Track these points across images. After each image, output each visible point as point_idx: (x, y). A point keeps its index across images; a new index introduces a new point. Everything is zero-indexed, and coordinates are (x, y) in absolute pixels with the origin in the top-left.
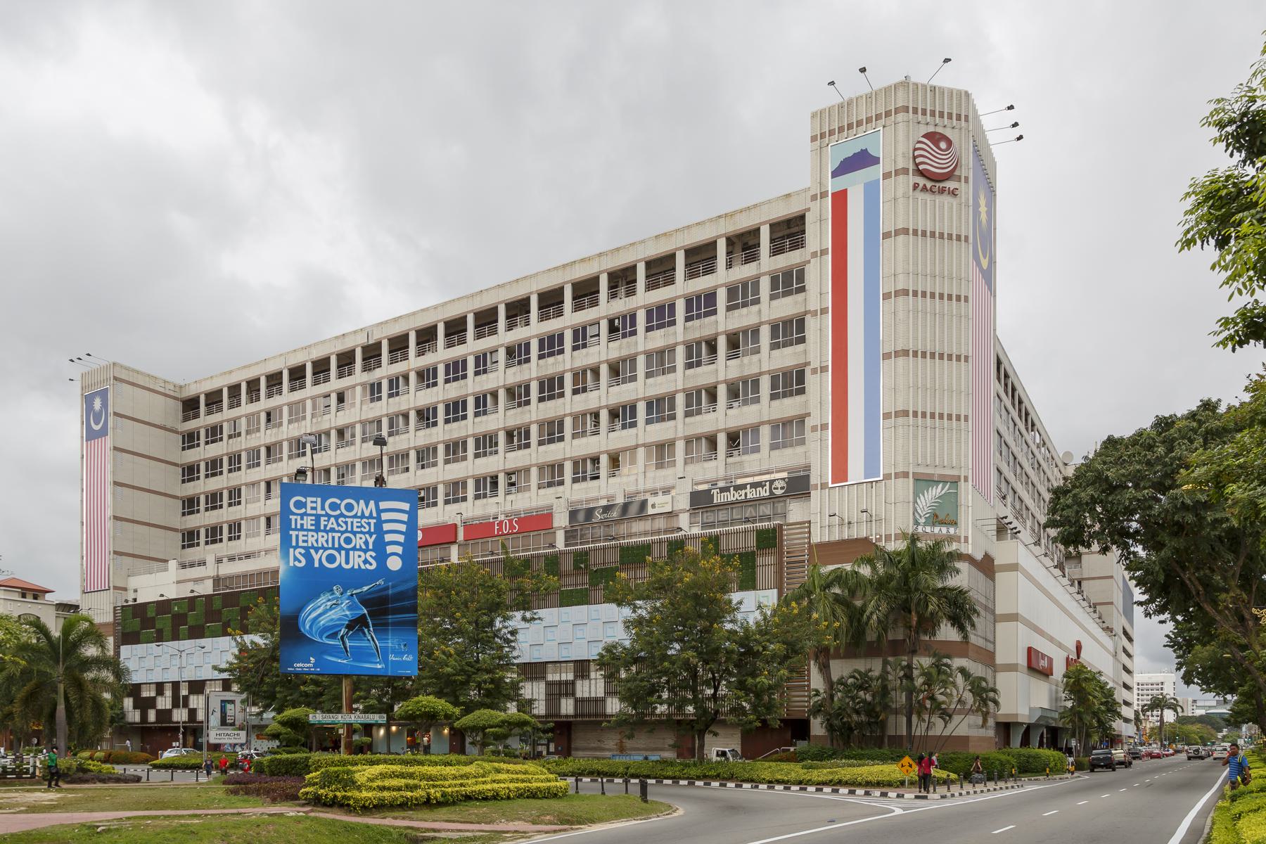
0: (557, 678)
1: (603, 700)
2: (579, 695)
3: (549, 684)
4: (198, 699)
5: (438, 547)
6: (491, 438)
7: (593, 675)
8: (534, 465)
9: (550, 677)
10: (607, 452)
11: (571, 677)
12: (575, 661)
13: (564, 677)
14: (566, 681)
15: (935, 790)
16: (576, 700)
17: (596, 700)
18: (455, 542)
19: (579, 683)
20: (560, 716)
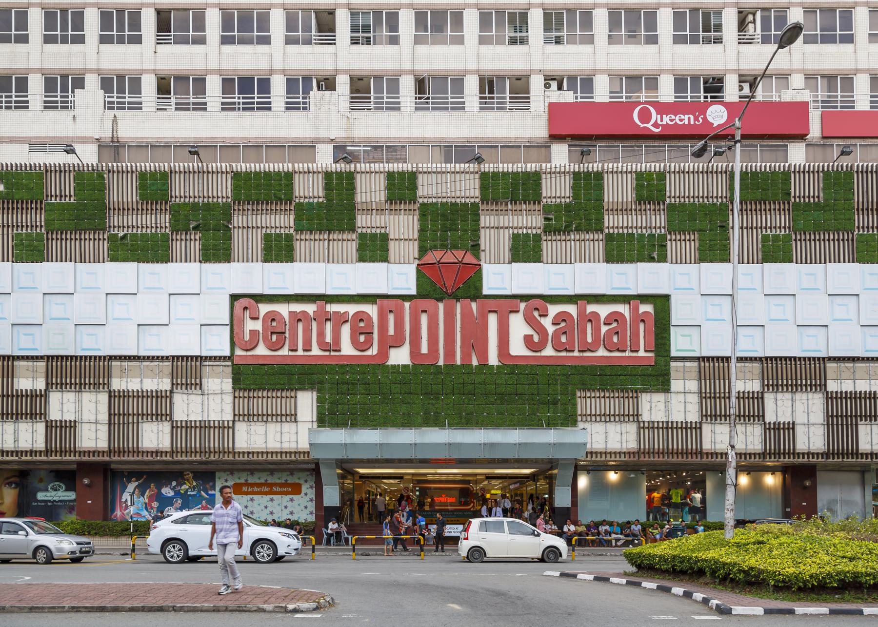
0: (847, 386)
1: (698, 427)
2: (770, 418)
3: (830, 398)
4: (79, 401)
5: (667, 144)
6: (707, 16)
7: (676, 385)
8: (798, 71)
9: (117, 384)
10: (219, 72)
11: (165, 385)
12: (49, 358)
13: (749, 388)
14: (703, 396)
15: (442, 548)
16: (49, 425)
17: (685, 427)
18: (801, 137)
19: (55, 397)
20: (856, 454)
